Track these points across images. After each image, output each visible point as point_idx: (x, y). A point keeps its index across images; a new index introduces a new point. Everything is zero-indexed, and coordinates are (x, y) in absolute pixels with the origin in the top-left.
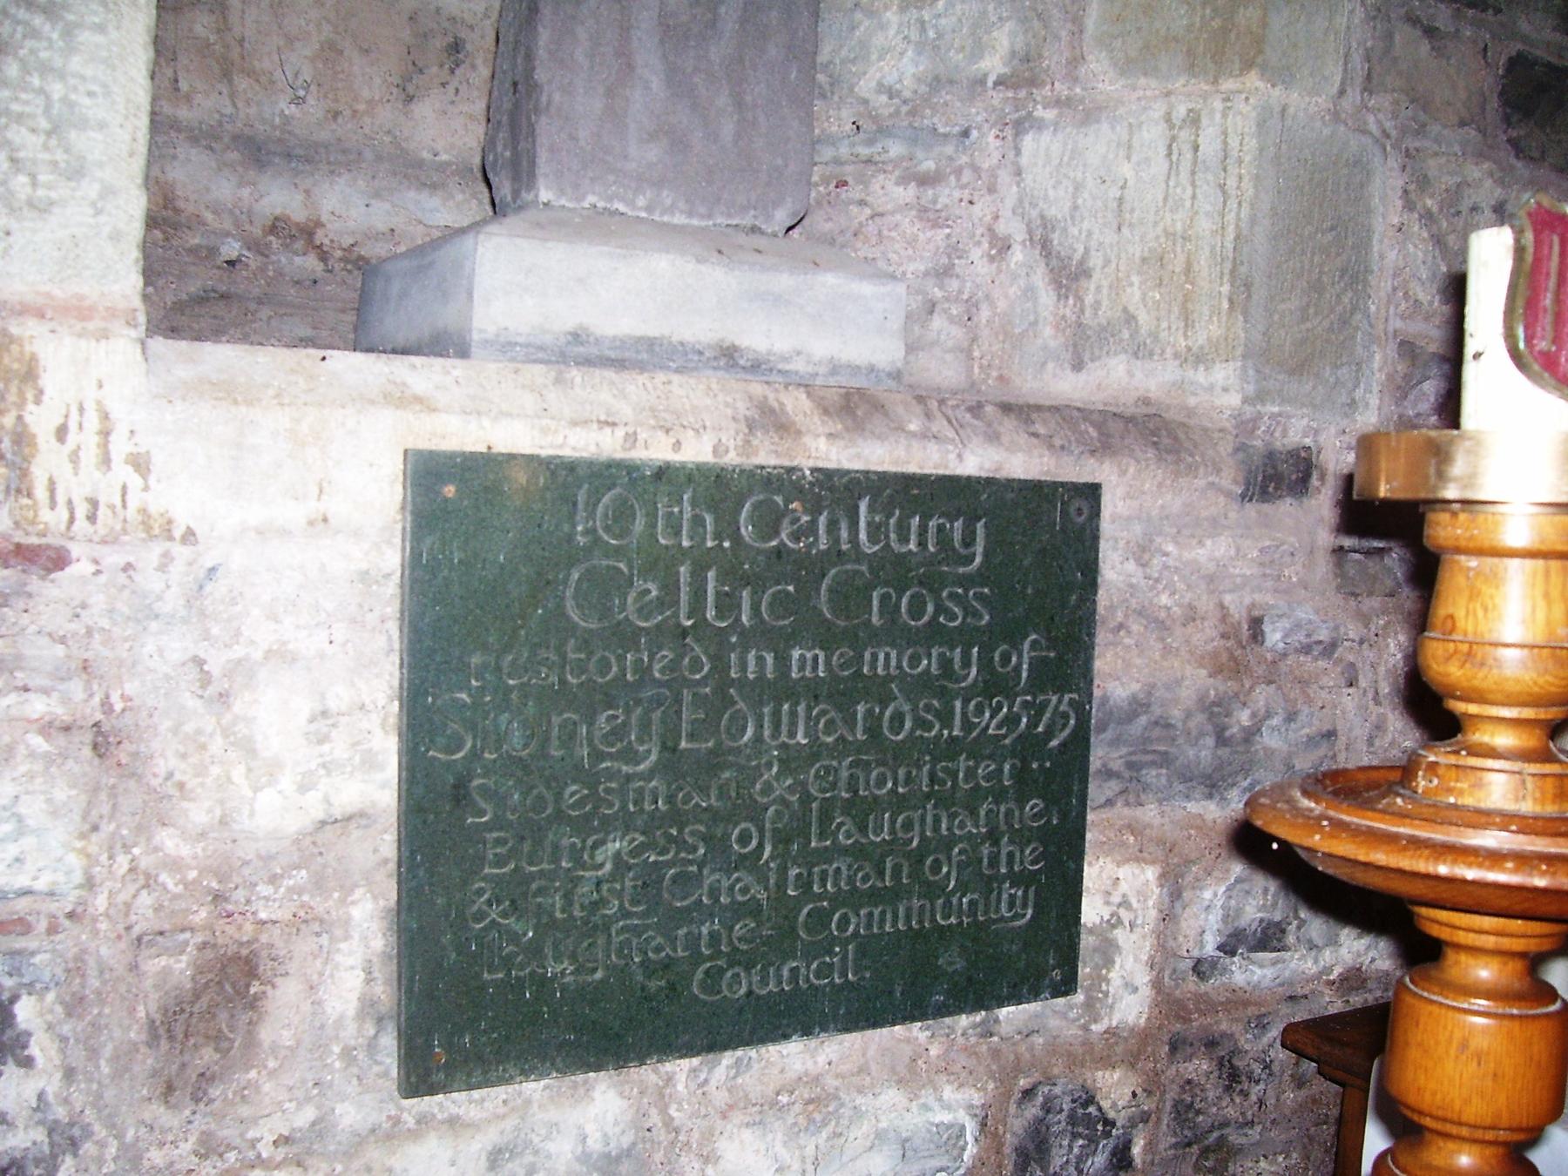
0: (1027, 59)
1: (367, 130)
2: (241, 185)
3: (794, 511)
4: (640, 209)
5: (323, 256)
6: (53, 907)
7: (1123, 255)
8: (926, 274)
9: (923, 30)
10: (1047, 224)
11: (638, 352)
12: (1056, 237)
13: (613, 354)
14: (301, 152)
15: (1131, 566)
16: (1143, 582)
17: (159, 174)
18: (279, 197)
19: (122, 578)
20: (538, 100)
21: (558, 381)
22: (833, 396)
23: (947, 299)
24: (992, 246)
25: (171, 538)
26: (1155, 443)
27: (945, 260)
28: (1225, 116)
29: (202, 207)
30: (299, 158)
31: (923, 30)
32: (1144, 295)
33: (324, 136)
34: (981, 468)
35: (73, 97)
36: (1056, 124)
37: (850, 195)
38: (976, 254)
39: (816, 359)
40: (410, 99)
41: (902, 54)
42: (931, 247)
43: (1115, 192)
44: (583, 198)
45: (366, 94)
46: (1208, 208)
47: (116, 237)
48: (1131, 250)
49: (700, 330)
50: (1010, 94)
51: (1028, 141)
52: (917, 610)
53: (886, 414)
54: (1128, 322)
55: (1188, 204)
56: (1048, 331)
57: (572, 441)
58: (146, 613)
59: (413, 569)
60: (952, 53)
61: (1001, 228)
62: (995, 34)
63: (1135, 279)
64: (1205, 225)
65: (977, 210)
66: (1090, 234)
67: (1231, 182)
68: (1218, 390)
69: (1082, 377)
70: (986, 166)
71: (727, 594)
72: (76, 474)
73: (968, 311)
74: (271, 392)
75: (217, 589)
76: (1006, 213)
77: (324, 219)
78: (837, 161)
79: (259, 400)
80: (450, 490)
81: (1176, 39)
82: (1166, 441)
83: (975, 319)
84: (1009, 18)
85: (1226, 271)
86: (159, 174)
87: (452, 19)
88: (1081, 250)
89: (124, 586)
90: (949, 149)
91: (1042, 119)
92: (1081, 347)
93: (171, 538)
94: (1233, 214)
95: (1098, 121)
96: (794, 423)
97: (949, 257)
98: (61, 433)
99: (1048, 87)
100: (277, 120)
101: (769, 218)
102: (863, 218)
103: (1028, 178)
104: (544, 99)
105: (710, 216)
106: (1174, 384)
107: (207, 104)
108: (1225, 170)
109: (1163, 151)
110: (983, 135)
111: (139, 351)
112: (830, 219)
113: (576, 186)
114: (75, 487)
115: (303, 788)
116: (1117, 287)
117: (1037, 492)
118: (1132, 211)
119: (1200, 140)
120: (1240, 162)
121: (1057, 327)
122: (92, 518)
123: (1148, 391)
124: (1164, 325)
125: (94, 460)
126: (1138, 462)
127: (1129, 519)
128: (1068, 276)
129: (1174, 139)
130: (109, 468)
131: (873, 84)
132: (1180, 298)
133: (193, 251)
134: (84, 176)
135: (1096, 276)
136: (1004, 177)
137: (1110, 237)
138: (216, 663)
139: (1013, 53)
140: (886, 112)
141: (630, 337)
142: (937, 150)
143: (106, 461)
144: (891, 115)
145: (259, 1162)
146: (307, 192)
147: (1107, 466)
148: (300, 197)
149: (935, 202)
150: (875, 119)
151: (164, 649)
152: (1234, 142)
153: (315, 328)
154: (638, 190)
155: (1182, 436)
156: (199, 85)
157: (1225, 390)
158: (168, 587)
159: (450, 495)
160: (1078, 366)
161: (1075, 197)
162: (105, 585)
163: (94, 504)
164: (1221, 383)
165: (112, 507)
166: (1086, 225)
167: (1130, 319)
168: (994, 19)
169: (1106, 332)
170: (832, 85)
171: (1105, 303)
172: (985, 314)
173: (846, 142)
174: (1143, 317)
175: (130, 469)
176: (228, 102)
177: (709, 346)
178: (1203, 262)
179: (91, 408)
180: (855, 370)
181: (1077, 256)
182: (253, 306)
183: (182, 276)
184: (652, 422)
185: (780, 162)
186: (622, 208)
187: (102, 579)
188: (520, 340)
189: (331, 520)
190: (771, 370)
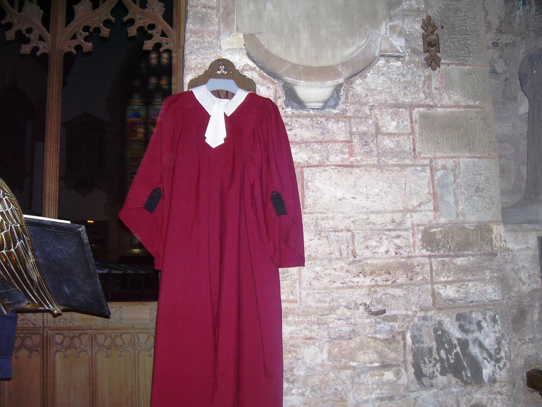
6: (499, 302)
58: (507, 262)
75: (515, 258)
98: (496, 238)
114: (498, 245)
115: (529, 285)
138: (516, 268)
143: (501, 241)
145: (527, 342)
151: (509, 267)
163: (500, 247)
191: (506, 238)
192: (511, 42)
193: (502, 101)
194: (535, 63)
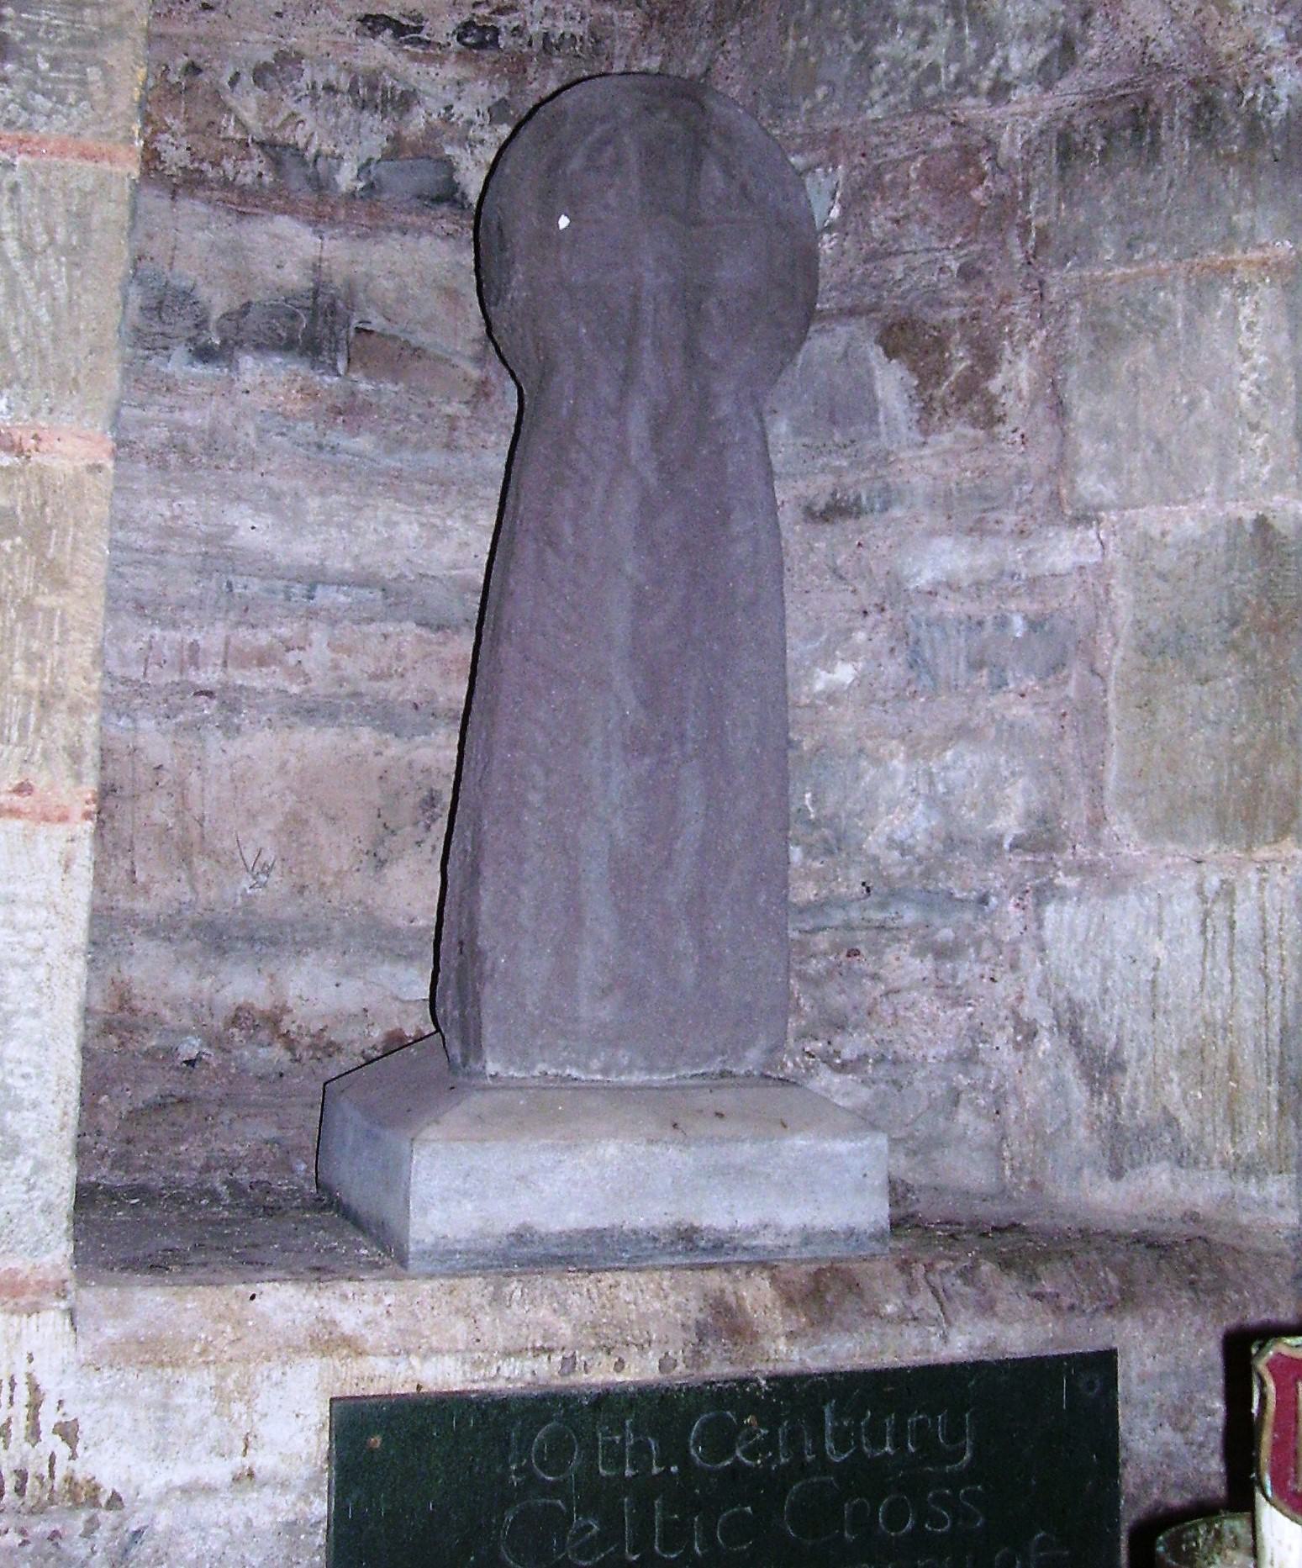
0: (1043, 821)
1: (335, 903)
2: (200, 976)
3: (750, 1425)
4: (596, 1072)
5: (290, 1045)
7: (1160, 1047)
8: (949, 1059)
9: (931, 784)
10: (1076, 1009)
11: (586, 1246)
12: (1085, 1024)
13: (558, 1252)
14: (264, 933)
15: (1167, 1433)
16: (1184, 1450)
17: (116, 974)
18: (242, 986)
19: (48, 1546)
20: (481, 968)
21: (497, 1299)
22: (800, 1277)
23: (973, 1087)
24: (1017, 1031)
25: (96, 1504)
26: (1192, 1283)
27: (968, 1044)
28: (1261, 888)
29: (161, 1005)
30: (262, 940)
31: (931, 784)
32: (1184, 1094)
33: (289, 911)
34: (971, 1347)
35: (9, 1081)
36: (1079, 893)
37: (863, 966)
38: (1000, 1039)
39: (786, 1230)
40: (382, 863)
41: (912, 808)
42: (953, 1027)
43: (1146, 974)
44: (533, 1066)
45: (334, 865)
46: (1250, 994)
47: (47, 1209)
48: (1168, 1041)
49: (652, 1214)
50: (1029, 858)
51: (1050, 912)
52: (895, 1521)
53: (860, 1295)
54: (1169, 1124)
55: (1227, 989)
56: (1082, 1132)
57: (506, 1371)
59: (337, 1527)
60: (964, 811)
61: (1026, 1011)
62: (1008, 791)
63: (1174, 1075)
64: (1247, 1015)
65: (999, 987)
66: (1122, 1022)
67: (1273, 966)
68: (1273, 1205)
69: (1123, 1184)
70: (1007, 938)
71: (675, 1522)
72: (6, 1448)
73: (996, 1103)
74: (197, 1349)
76: (1031, 994)
77: (290, 1005)
78: (849, 927)
79: (185, 1359)
80: (376, 1441)
81: (1203, 800)
82: (1207, 1276)
83: (1003, 1113)
84: (1022, 774)
85: (1273, 1068)
86: (116, 974)
87: (426, 771)
88: (1114, 1039)
89: (51, 1554)
90: (968, 916)
91: (1064, 887)
92: (1121, 1150)
93: (96, 1504)
94: (1277, 1002)
95: (1124, 892)
96: (749, 1323)
97: (973, 1041)
99: (1070, 851)
100: (239, 899)
101: (739, 1060)
102: (876, 994)
103: (1052, 954)
104: (488, 966)
105: (671, 1069)
106: (1223, 1197)
107: (165, 890)
108: (1265, 952)
109: (1195, 928)
110: (1003, 903)
111: (68, 1321)
112: (842, 992)
113: (524, 1054)
116: (1156, 1083)
117: (1034, 1374)
118: (1167, 995)
119: (1236, 916)
120: (1281, 941)
121: (1091, 1127)
122: (20, 1490)
123: (1195, 1205)
124: (1209, 1128)
125: (23, 1433)
126: (1169, 1311)
127: (1162, 1375)
128: (1101, 1069)
129: (1207, 914)
130: (38, 1440)
131: (882, 840)
132: (1224, 1098)
133: (150, 1054)
134: (18, 1154)
135: (1132, 1069)
136: (1026, 950)
137: (1144, 1026)
139: (1029, 814)
140: (897, 872)
141: (577, 1231)
142: (956, 916)
143: (34, 1433)
144: (902, 877)
146: (272, 976)
147: (1128, 1322)
148: (264, 983)
149: (954, 977)
150: (887, 881)
152: (1273, 921)
153: (281, 1128)
154: (591, 1054)
155: (1229, 1266)
156: (159, 875)
157: (1281, 1206)
158: (94, 1553)
159: (381, 1446)
160: (1117, 1174)
161: (1103, 979)
162: (32, 1554)
163: (22, 1475)
164: (1275, 1197)
165: (40, 1478)
166: (1116, 1011)
167: (1171, 1121)
168: (1006, 773)
169: (1146, 1135)
170: (838, 840)
171: (1143, 1101)
172: (1012, 1110)
173: (856, 905)
174: (1184, 1119)
175: (58, 1438)
176: (187, 888)
177: (665, 1231)
178: (1246, 1058)
179: (21, 1380)
180: (830, 1236)
181: (1110, 1046)
182: (213, 1110)
183: (140, 1080)
184: (593, 1343)
185: (748, 998)
186: (575, 1073)
187: (29, 1548)
188: (458, 1247)
189: (259, 1476)
190: (735, 1249)
191: (72, 1411)
192: (579, 31)
193: (475, 373)
194: (576, 164)
